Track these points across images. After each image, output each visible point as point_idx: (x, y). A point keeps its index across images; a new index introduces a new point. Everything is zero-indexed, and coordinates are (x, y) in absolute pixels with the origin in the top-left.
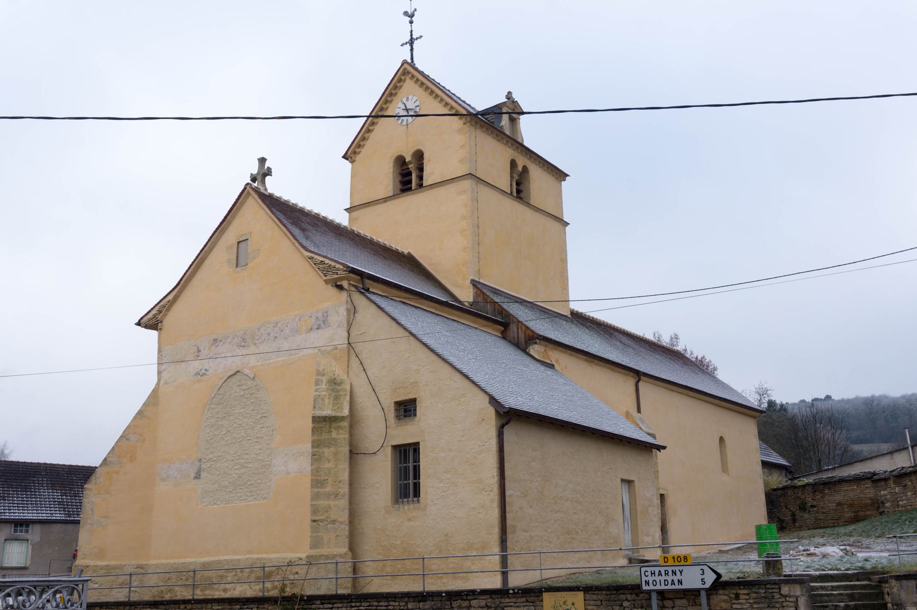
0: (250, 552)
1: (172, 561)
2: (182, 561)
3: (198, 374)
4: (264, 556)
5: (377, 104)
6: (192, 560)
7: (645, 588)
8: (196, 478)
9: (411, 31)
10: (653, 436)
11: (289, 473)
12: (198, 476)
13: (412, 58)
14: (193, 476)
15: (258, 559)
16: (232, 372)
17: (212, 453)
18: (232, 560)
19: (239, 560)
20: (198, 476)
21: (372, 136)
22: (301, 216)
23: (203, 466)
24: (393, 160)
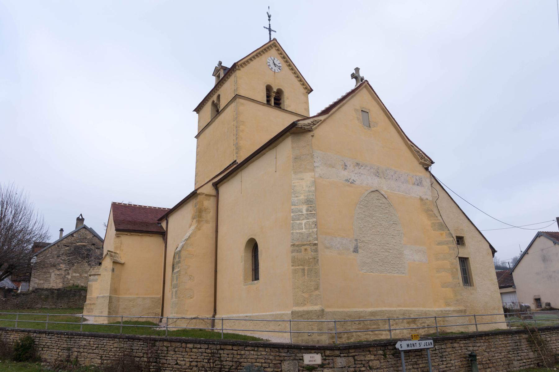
0: (399, 306)
1: (347, 310)
2: (355, 310)
3: (347, 180)
4: (409, 309)
5: (258, 49)
6: (362, 310)
7: (432, 341)
8: (354, 251)
9: (269, 20)
10: (137, 294)
11: (415, 261)
12: (356, 250)
13: (270, 34)
14: (352, 249)
15: (406, 310)
16: (374, 190)
17: (364, 237)
18: (390, 311)
19: (395, 311)
20: (356, 250)
21: (252, 63)
22: (273, 95)
23: (359, 245)
24: (283, 90)
